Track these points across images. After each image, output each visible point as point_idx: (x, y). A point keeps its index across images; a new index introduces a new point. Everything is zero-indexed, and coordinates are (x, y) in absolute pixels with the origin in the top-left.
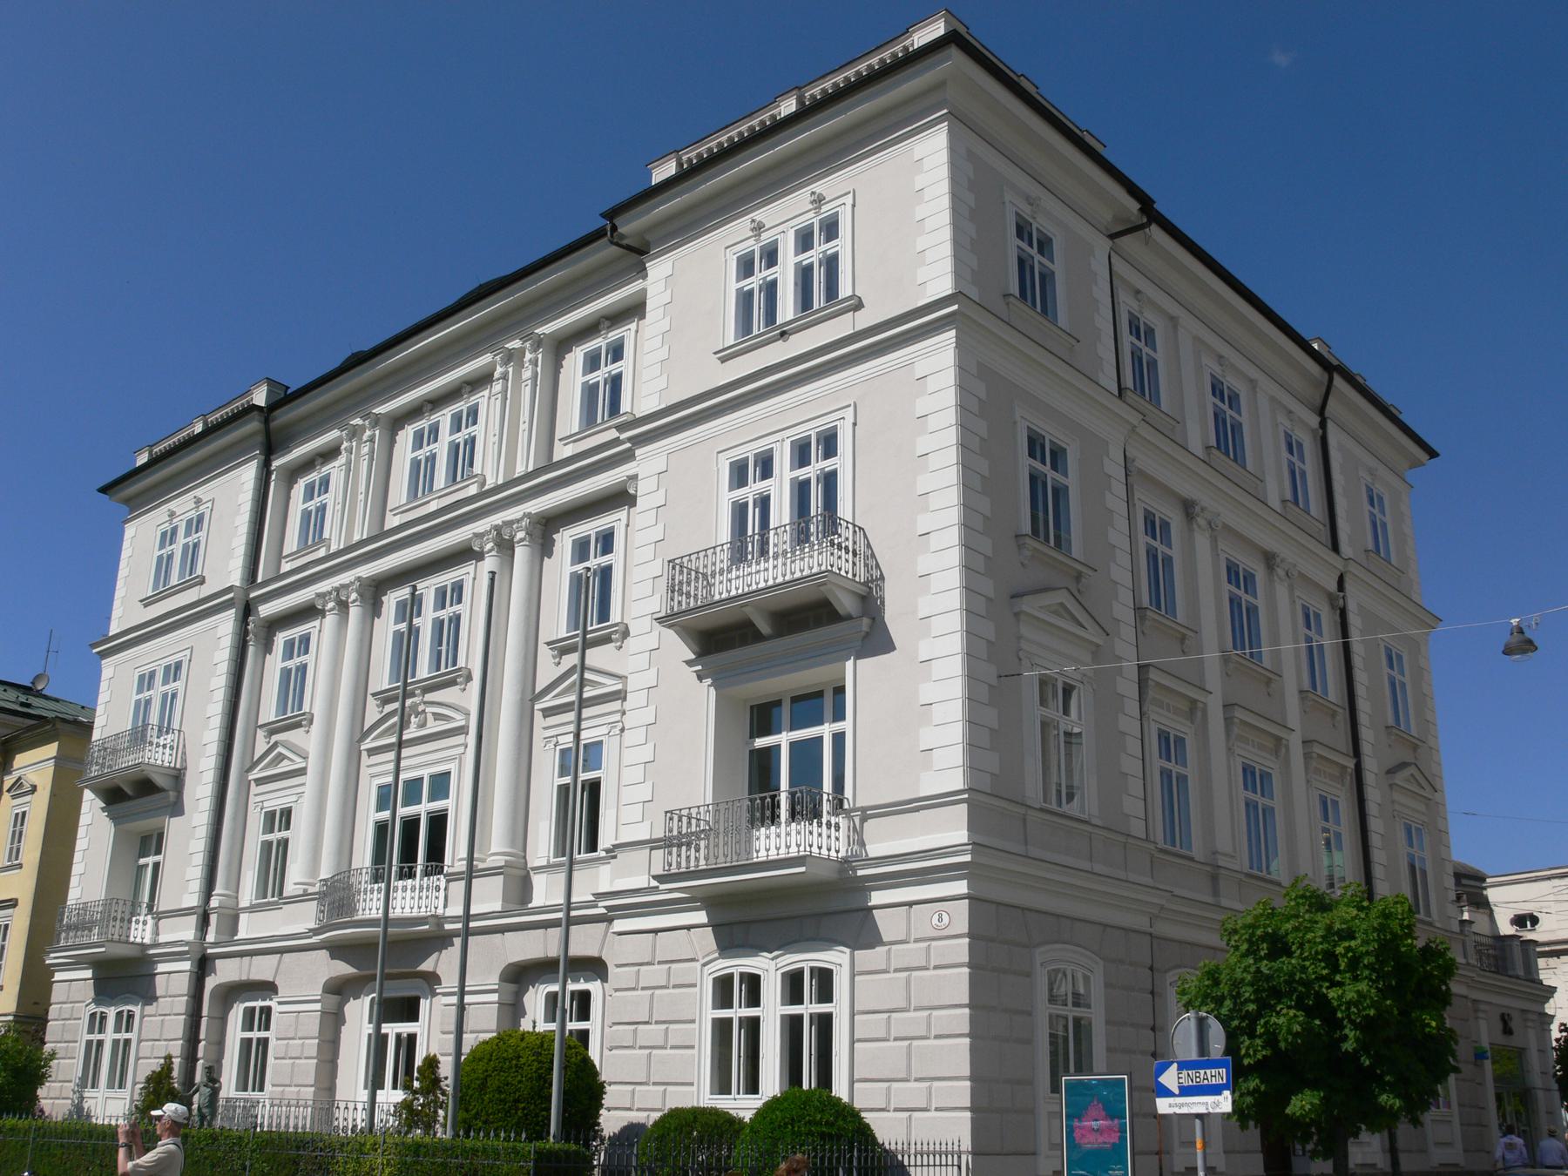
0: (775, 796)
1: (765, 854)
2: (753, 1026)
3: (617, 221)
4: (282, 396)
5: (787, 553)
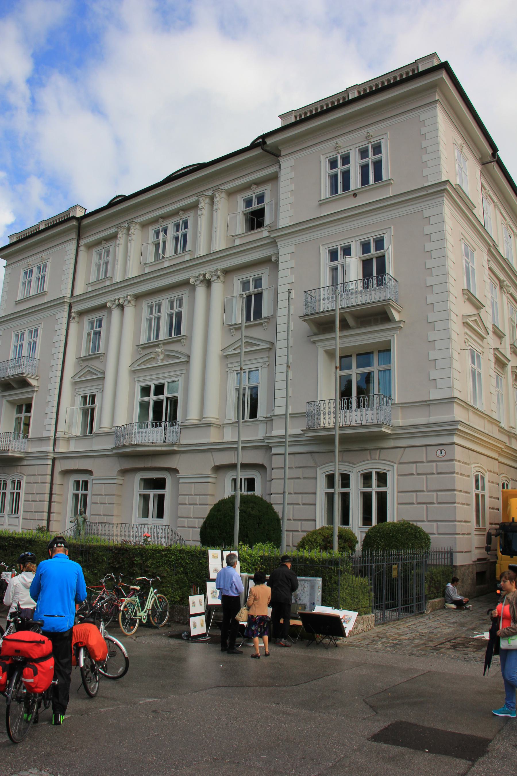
0: (349, 399)
1: (323, 425)
2: (345, 497)
3: (266, 140)
4: (84, 214)
5: (329, 298)
